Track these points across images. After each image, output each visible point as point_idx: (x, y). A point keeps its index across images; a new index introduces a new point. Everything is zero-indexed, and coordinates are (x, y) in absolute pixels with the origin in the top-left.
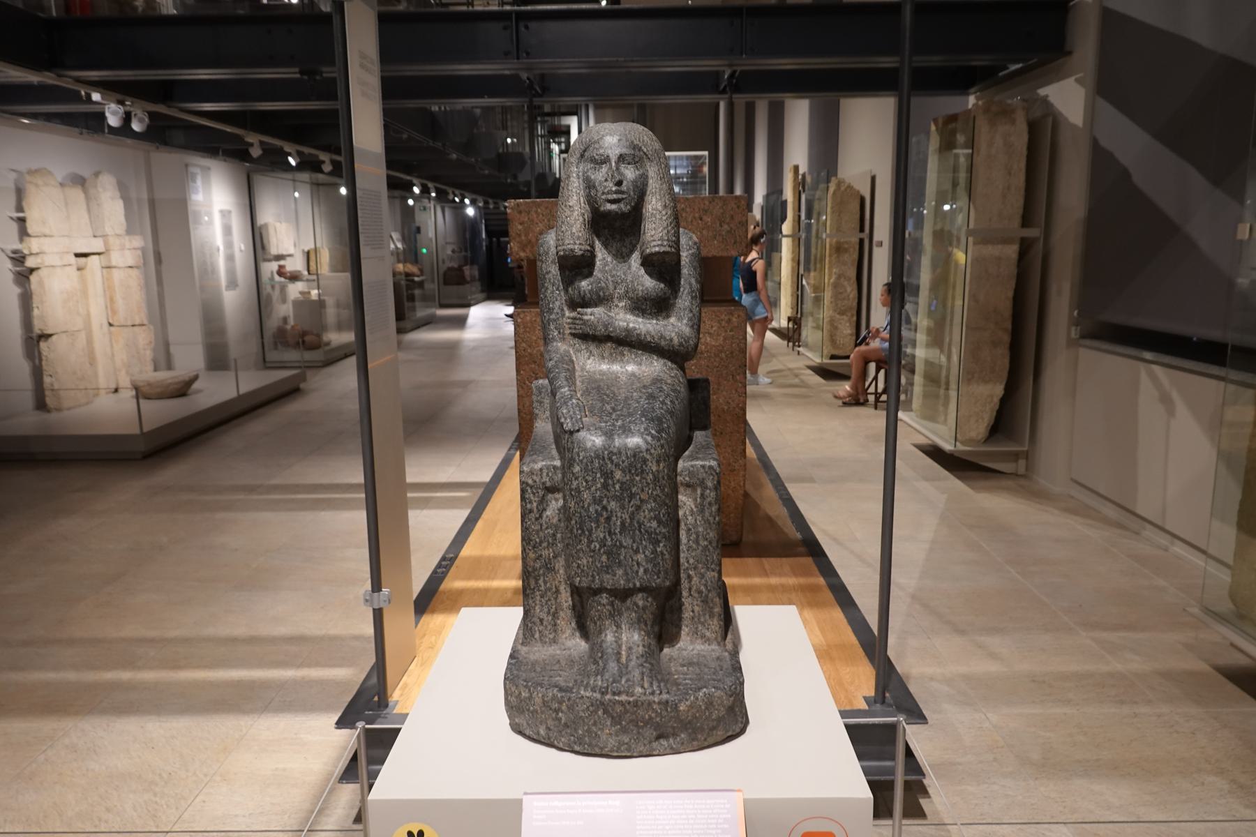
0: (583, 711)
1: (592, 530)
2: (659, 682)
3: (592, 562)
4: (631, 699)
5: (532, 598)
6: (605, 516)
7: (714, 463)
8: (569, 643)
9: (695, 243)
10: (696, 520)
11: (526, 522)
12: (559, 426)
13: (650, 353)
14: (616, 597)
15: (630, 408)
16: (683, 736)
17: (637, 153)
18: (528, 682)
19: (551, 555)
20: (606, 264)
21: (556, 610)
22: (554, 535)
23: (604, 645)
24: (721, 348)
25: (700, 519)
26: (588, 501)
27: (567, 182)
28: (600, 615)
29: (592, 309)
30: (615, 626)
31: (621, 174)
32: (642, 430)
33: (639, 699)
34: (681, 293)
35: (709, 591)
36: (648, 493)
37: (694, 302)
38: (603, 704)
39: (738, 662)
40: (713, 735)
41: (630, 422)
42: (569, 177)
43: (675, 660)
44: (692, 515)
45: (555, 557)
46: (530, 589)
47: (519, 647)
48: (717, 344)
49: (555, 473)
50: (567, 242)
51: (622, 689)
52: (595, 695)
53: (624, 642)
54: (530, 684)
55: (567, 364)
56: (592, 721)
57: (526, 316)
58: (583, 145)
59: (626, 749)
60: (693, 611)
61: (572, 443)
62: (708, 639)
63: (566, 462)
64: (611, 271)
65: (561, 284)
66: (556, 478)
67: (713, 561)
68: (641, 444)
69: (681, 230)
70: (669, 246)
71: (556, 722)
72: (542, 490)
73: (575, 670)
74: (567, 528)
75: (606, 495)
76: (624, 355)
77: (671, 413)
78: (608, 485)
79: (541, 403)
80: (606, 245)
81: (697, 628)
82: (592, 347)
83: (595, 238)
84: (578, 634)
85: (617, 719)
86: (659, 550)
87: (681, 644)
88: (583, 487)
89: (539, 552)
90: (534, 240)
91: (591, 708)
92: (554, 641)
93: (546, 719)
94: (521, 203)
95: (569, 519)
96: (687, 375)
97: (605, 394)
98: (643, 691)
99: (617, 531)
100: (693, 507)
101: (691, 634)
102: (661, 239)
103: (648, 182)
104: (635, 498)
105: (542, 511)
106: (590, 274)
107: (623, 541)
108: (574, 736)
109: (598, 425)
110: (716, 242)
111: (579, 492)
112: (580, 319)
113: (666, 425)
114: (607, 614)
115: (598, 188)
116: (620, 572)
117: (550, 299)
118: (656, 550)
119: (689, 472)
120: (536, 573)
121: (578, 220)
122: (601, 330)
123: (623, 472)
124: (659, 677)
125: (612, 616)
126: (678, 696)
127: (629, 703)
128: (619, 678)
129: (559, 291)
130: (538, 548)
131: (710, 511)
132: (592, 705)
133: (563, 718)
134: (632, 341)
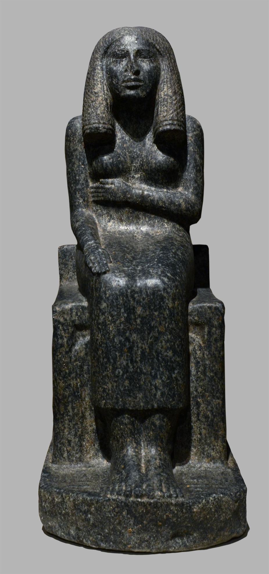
0: (110, 512)
1: (116, 357)
2: (175, 488)
3: (116, 386)
5: (62, 422)
6: (128, 346)
8: (93, 462)
10: (203, 354)
11: (58, 356)
14: (136, 418)
15: (147, 257)
18: (60, 489)
19: (79, 384)
21: (82, 433)
22: (81, 367)
23: (126, 459)
27: (93, 73)
28: (122, 433)
29: (112, 180)
30: (135, 442)
31: (139, 66)
34: (187, 167)
36: (165, 327)
38: (128, 506)
39: (240, 476)
40: (220, 535)
41: (148, 267)
43: (185, 474)
44: (200, 350)
45: (82, 386)
47: (50, 465)
50: (92, 121)
53: (143, 457)
54: (62, 491)
55: (91, 224)
56: (117, 521)
58: (106, 43)
59: (147, 546)
60: (200, 434)
61: (100, 283)
64: (128, 148)
65: (86, 160)
66: (84, 317)
67: (218, 391)
68: (159, 284)
70: (178, 125)
71: (85, 523)
72: (72, 327)
73: (100, 481)
74: (94, 358)
77: (183, 262)
78: (131, 319)
80: (125, 127)
81: (203, 449)
84: (100, 455)
86: (174, 376)
89: (69, 382)
92: (80, 460)
95: (96, 350)
97: (126, 247)
98: (162, 494)
99: (138, 360)
100: (201, 343)
102: (172, 119)
103: (160, 73)
105: (72, 346)
107: (143, 368)
108: (101, 535)
111: (106, 326)
112: (102, 188)
113: (179, 271)
114: (129, 433)
115: (120, 77)
116: (140, 395)
117: (76, 172)
118: (172, 376)
121: (102, 104)
124: (175, 484)
125: (132, 434)
126: (192, 499)
127: (150, 504)
129: (84, 165)
130: (67, 378)
132: (118, 507)
133: (92, 519)
134: (146, 206)
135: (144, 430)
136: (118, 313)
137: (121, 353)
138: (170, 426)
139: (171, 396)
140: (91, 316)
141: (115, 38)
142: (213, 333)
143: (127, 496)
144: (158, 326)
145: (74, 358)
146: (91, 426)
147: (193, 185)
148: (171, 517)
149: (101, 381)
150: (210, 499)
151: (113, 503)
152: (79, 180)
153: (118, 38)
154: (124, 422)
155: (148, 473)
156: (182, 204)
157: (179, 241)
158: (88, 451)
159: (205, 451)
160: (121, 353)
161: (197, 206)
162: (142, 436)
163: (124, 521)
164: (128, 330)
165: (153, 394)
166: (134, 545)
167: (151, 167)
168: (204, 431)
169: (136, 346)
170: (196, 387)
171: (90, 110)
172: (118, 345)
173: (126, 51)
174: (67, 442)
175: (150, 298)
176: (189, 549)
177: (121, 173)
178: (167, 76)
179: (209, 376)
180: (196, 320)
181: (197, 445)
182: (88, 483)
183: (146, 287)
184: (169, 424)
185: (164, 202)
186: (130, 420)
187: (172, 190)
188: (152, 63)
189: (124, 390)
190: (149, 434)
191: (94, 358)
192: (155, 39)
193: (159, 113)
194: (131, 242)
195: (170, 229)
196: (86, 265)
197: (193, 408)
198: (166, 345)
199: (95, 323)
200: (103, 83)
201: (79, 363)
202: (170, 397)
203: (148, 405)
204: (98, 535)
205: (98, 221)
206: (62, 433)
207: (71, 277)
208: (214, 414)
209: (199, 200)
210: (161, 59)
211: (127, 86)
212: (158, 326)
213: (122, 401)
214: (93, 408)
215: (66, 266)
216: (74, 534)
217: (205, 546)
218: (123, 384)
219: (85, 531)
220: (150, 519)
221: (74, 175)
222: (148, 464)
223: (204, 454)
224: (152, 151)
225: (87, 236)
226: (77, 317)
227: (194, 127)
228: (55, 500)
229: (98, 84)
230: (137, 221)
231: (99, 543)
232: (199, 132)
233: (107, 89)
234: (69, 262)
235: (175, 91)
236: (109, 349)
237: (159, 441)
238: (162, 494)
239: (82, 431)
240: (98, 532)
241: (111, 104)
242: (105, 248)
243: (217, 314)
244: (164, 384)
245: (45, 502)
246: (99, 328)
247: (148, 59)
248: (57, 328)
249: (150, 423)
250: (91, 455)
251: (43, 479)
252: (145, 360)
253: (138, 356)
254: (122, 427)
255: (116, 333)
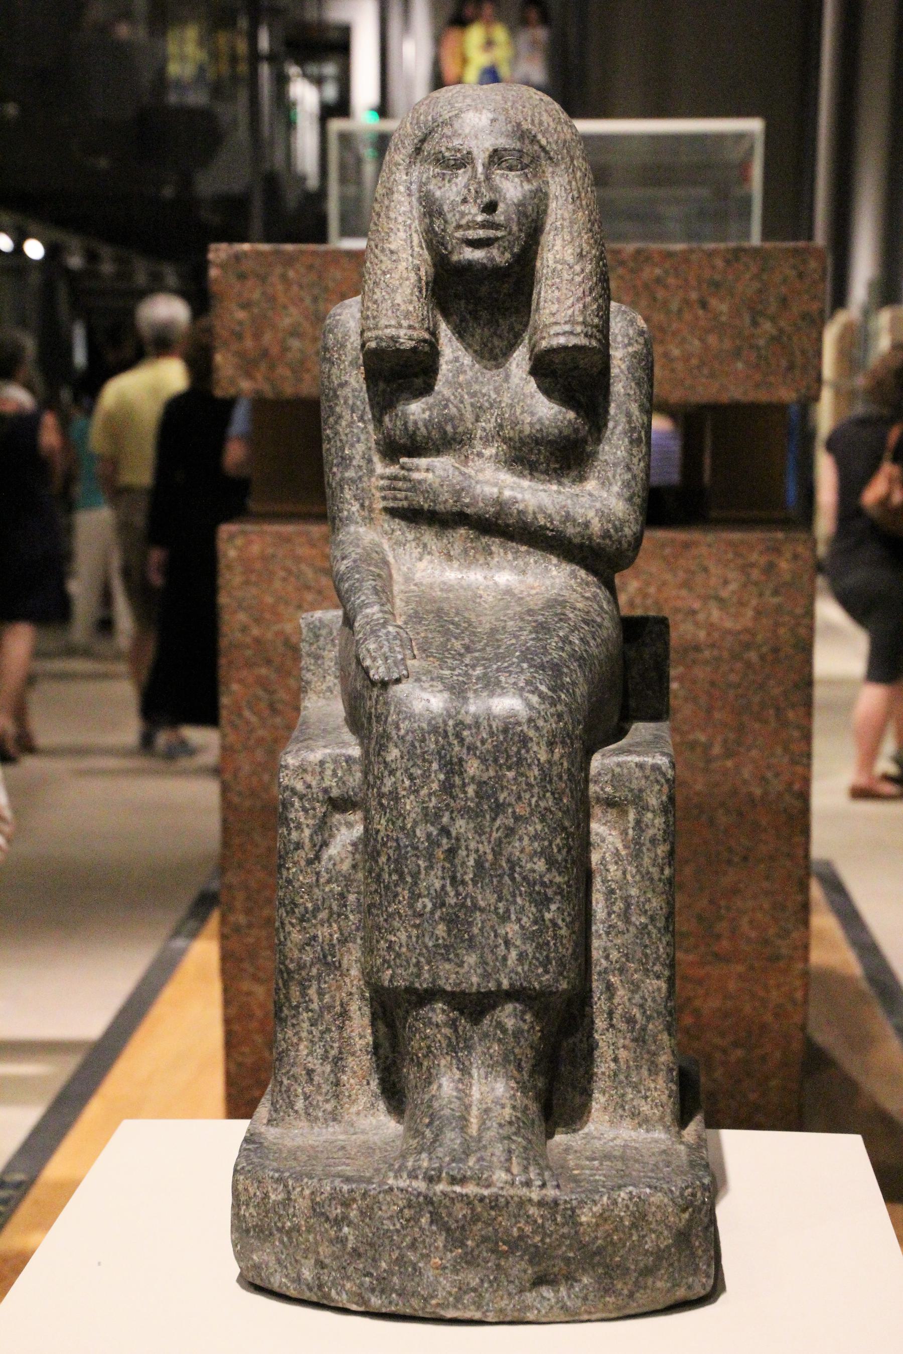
0: (391, 1218)
1: (419, 872)
2: (541, 1168)
3: (418, 937)
4: (486, 1192)
5: (293, 1025)
6: (446, 847)
7: (662, 761)
9: (641, 333)
10: (624, 873)
11: (288, 869)
12: (362, 674)
13: (544, 550)
14: (462, 1013)
15: (499, 647)
16: (585, 1280)
17: (528, 147)
18: (283, 1172)
19: (336, 936)
20: (460, 371)
21: (340, 1053)
22: (342, 896)
23: (436, 1105)
24: (746, 638)
25: (634, 871)
26: (414, 815)
27: (386, 202)
28: (429, 1047)
30: (458, 1068)
31: (493, 189)
32: (522, 684)
33: (500, 1192)
34: (608, 432)
35: (649, 1018)
36: (530, 805)
37: (635, 451)
38: (431, 1202)
41: (498, 670)
42: (390, 192)
43: (576, 1152)
44: (616, 863)
46: (291, 1007)
48: (739, 627)
49: (350, 769)
50: (383, 322)
51: (469, 1173)
52: (415, 1184)
53: (475, 1103)
54: (287, 1174)
55: (376, 566)
56: (408, 1239)
57: (250, 542)
59: (474, 1303)
60: (616, 1060)
61: (386, 703)
62: (646, 1120)
63: (373, 742)
64: (469, 384)
65: (368, 408)
67: (658, 958)
68: (518, 708)
69: (614, 305)
70: (586, 335)
71: (337, 1248)
72: (323, 803)
74: (370, 872)
75: (448, 805)
76: (491, 553)
77: (581, 660)
78: (453, 786)
79: (317, 657)
80: (460, 333)
81: (623, 1095)
82: (429, 536)
83: (439, 317)
84: (382, 1106)
85: (457, 1234)
86: (548, 916)
87: (590, 1127)
88: (405, 789)
89: (312, 932)
90: (275, 351)
91: (407, 1213)
92: (334, 1116)
93: (316, 1243)
94: (245, 254)
95: (374, 856)
96: (623, 599)
98: (509, 1177)
99: (467, 878)
100: (620, 846)
101: (611, 1109)
102: (571, 321)
103: (547, 206)
104: (504, 813)
105: (321, 846)
106: (427, 389)
107: (479, 897)
108: (371, 1275)
109: (436, 673)
110: (740, 365)
111: (397, 799)
112: (405, 479)
113: (568, 679)
114: (444, 1045)
115: (449, 216)
116: (471, 959)
117: (344, 438)
118: (543, 916)
119: (613, 775)
120: (304, 973)
122: (446, 502)
123: (482, 762)
125: (453, 1049)
127: (482, 1199)
128: (463, 1156)
129: (364, 422)
130: (308, 921)
131: (653, 855)
132: (410, 1206)
133: (351, 1237)
134: (508, 526)
135: (480, 1040)
136: (425, 771)
137: (431, 862)
138: (539, 1034)
139: (540, 963)
140: (366, 777)
141: (441, 116)
142: (647, 825)
143: (431, 1180)
144: (514, 803)
145: (325, 874)
146: (361, 1037)
147: (620, 475)
148: (528, 1233)
149: (385, 925)
150: (619, 1195)
151: (401, 1196)
152: (351, 458)
153: (447, 117)
154: (434, 1020)
155: (484, 1134)
156: (592, 521)
157: (579, 610)
158: (353, 1097)
159: (626, 1102)
160: (431, 862)
161: (630, 527)
162: (474, 1055)
163: (424, 1241)
164: (447, 810)
165: (500, 957)
166: (445, 1298)
167: (521, 432)
168: (623, 1054)
169: (463, 848)
170: (605, 949)
171: (378, 293)
172: (422, 843)
173: (465, 152)
174: (304, 1072)
175: (496, 741)
176: (572, 1317)
177: (451, 444)
178: (562, 215)
179: (638, 923)
180: (609, 795)
181: (609, 1086)
182: (347, 1161)
183: (489, 715)
184: (538, 1028)
185: (550, 516)
186: (448, 1015)
187: (570, 487)
188: (529, 181)
189: (434, 946)
190: (491, 1051)
191: (370, 872)
192: (536, 122)
193: (542, 304)
194: (467, 609)
195: (563, 580)
196: (359, 662)
197: (599, 999)
198: (531, 845)
199: (373, 795)
200: (410, 228)
201: (338, 886)
202: (537, 964)
203: (489, 982)
204: (365, 1276)
205: (394, 557)
206: (293, 1053)
207: (330, 690)
208: (648, 1012)
209: (635, 512)
210: (551, 169)
211: (467, 239)
212: (514, 803)
213: (429, 971)
214: (367, 995)
215: (319, 662)
216: (309, 1279)
217: (611, 1312)
218: (433, 933)
219: (335, 1267)
220: (482, 1236)
221: (339, 444)
222: (485, 1117)
223: (624, 1110)
224: (524, 394)
225: (363, 594)
226: (336, 780)
227: (628, 335)
228: (269, 1198)
229: (398, 230)
230: (486, 559)
231: (367, 1295)
232: (640, 347)
233: (420, 242)
234: (326, 652)
235: (582, 250)
236: (403, 851)
237: (512, 1067)
238: (509, 1177)
239: (340, 1048)
240: (364, 1268)
241: (430, 279)
242: (406, 623)
243: (657, 782)
244: (525, 934)
245: (247, 1205)
246: (381, 805)
247: (519, 173)
248: (289, 806)
249: (494, 1023)
250: (360, 1108)
251: (244, 1153)
252: (484, 879)
253: (468, 871)
254: (428, 1031)
255: (420, 817)
